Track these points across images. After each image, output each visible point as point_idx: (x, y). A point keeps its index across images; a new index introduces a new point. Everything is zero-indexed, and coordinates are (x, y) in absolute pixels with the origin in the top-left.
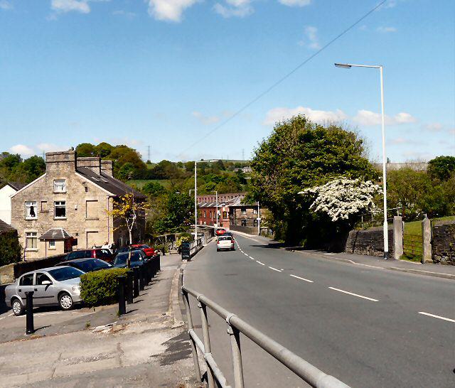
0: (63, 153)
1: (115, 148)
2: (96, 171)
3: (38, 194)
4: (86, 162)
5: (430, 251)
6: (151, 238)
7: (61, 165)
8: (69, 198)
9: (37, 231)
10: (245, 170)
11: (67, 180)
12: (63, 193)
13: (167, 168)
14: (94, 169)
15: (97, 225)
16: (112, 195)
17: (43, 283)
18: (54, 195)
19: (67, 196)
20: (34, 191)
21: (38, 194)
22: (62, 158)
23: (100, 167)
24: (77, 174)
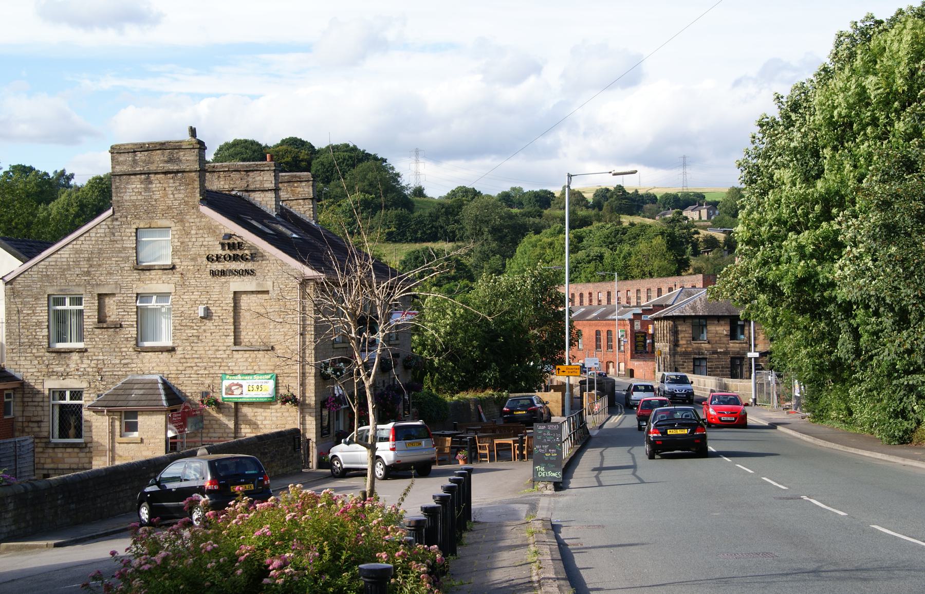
0: (162, 146)
1: (320, 152)
2: (266, 202)
3: (88, 273)
4: (235, 175)
5: (308, 427)
6: (196, 545)
7: (157, 183)
8: (183, 285)
9: (84, 385)
10: (691, 214)
11: (175, 227)
12: (164, 269)
13: (470, 210)
14: (258, 198)
15: (384, 431)
16: (309, 272)
17: (844, 253)
18: (135, 274)
19: (176, 277)
20: (77, 263)
21: (88, 273)
22: (159, 160)
23: (276, 190)
24: (205, 210)
